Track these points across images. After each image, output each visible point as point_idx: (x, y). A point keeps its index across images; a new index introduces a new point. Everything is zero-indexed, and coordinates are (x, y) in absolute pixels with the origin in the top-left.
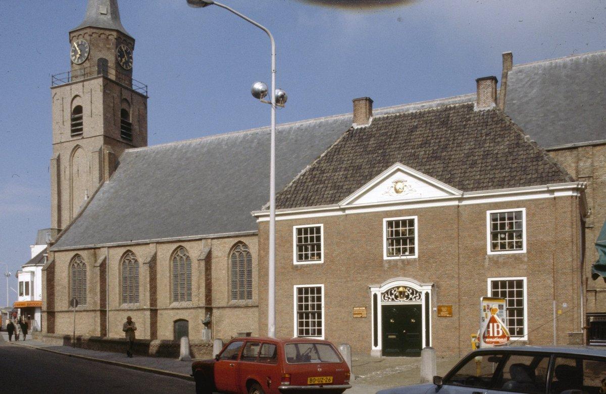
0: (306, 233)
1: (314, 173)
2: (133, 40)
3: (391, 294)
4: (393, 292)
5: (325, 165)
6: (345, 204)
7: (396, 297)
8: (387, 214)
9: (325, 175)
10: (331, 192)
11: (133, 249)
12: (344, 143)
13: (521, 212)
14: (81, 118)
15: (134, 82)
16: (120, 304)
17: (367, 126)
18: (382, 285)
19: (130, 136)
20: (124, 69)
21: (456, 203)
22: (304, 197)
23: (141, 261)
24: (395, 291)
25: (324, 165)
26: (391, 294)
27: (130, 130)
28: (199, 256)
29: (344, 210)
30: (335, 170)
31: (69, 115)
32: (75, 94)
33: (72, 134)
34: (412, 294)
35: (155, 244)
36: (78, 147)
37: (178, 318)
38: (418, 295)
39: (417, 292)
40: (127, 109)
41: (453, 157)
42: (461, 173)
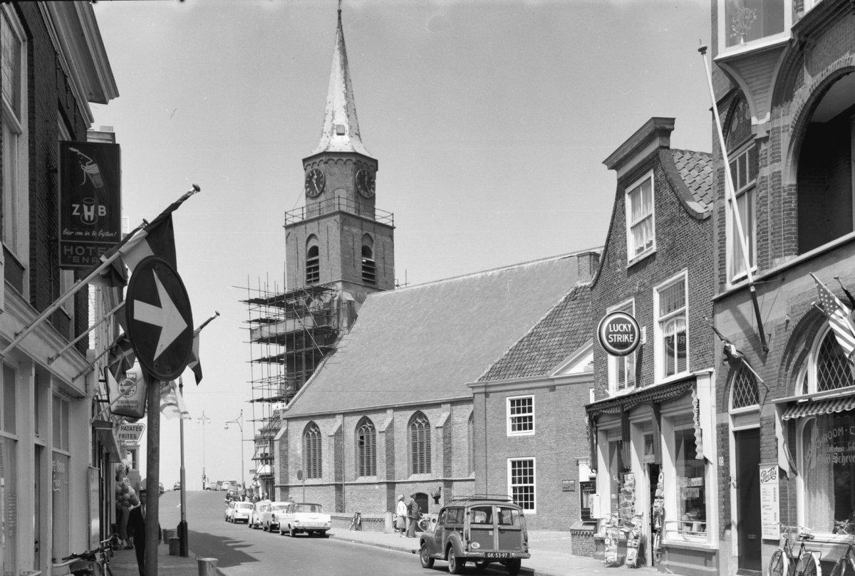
5: (543, 329)
9: (541, 341)
10: (544, 360)
14: (317, 261)
15: (377, 212)
19: (373, 277)
22: (517, 366)
23: (377, 428)
27: (372, 270)
31: (304, 257)
32: (310, 233)
33: (310, 260)
35: (449, 405)
37: (417, 491)
40: (369, 246)
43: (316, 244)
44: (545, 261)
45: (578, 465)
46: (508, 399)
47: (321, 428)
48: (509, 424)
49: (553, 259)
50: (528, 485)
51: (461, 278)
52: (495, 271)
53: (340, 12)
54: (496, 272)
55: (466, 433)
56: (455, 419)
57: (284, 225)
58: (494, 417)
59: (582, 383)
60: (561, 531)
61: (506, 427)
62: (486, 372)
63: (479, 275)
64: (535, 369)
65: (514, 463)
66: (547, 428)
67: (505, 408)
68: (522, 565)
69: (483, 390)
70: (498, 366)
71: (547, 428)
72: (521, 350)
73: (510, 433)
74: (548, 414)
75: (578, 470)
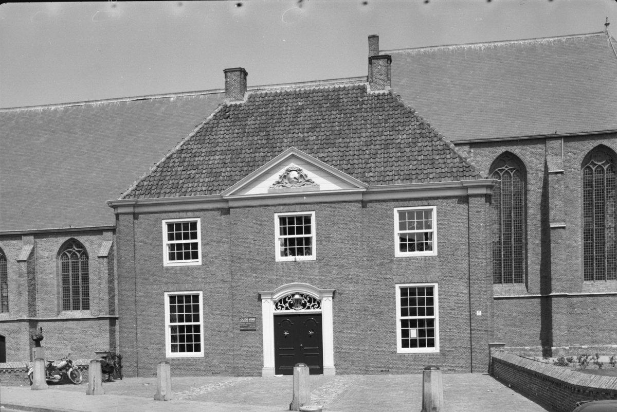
0: (180, 301)
1: (183, 156)
3: (285, 302)
4: (287, 299)
6: (228, 195)
10: (207, 180)
11: (82, 239)
12: (216, 122)
13: (432, 210)
17: (242, 102)
25: (195, 147)
30: (210, 153)
34: (310, 302)
35: (32, 237)
38: (316, 303)
39: (315, 300)
41: (351, 144)
42: (384, 158)
44: (116, 101)
45: (260, 300)
46: (164, 222)
48: (166, 251)
49: (124, 100)
50: (192, 323)
51: (18, 110)
52: (59, 107)
54: (61, 108)
55: (55, 269)
56: (40, 252)
58: (145, 243)
59: (265, 206)
60: (238, 376)
61: (162, 255)
62: (130, 189)
63: (40, 109)
64: (199, 189)
65: (172, 298)
66: (217, 257)
67: (161, 233)
69: (131, 210)
70: (145, 183)
71: (217, 257)
72: (173, 167)
73: (167, 262)
74: (219, 242)
75: (260, 307)
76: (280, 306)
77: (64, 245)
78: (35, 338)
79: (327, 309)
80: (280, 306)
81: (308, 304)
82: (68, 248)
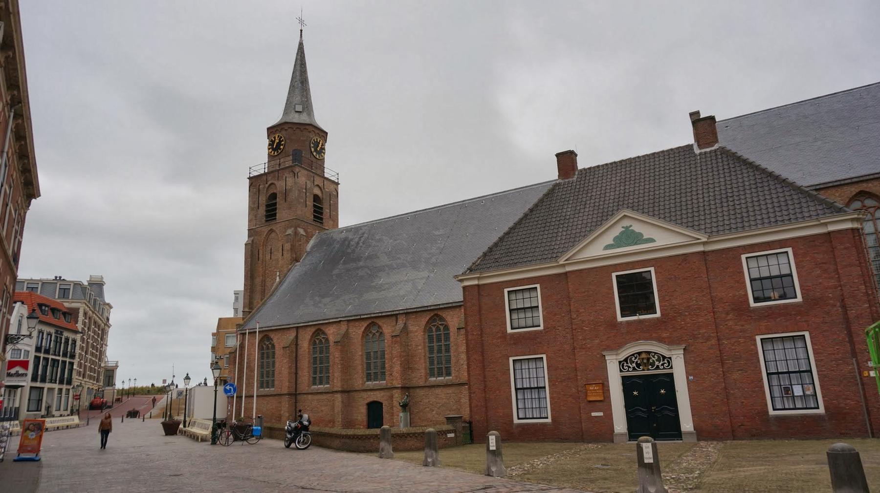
2: (324, 134)
3: (632, 362)
4: (633, 359)
7: (638, 365)
8: (616, 267)
11: (377, 321)
16: (309, 386)
18: (619, 352)
20: (317, 158)
21: (701, 248)
23: (331, 339)
24: (636, 358)
26: (632, 362)
27: (321, 214)
28: (393, 332)
29: (563, 266)
34: (659, 360)
36: (272, 231)
37: (371, 400)
38: (666, 361)
39: (664, 358)
43: (275, 191)
47: (275, 341)
53: (301, 31)
57: (248, 177)
68: (682, 430)
76: (626, 366)
77: (314, 333)
78: (401, 404)
79: (451, 377)
80: (626, 366)
81: (657, 363)
82: (432, 323)
